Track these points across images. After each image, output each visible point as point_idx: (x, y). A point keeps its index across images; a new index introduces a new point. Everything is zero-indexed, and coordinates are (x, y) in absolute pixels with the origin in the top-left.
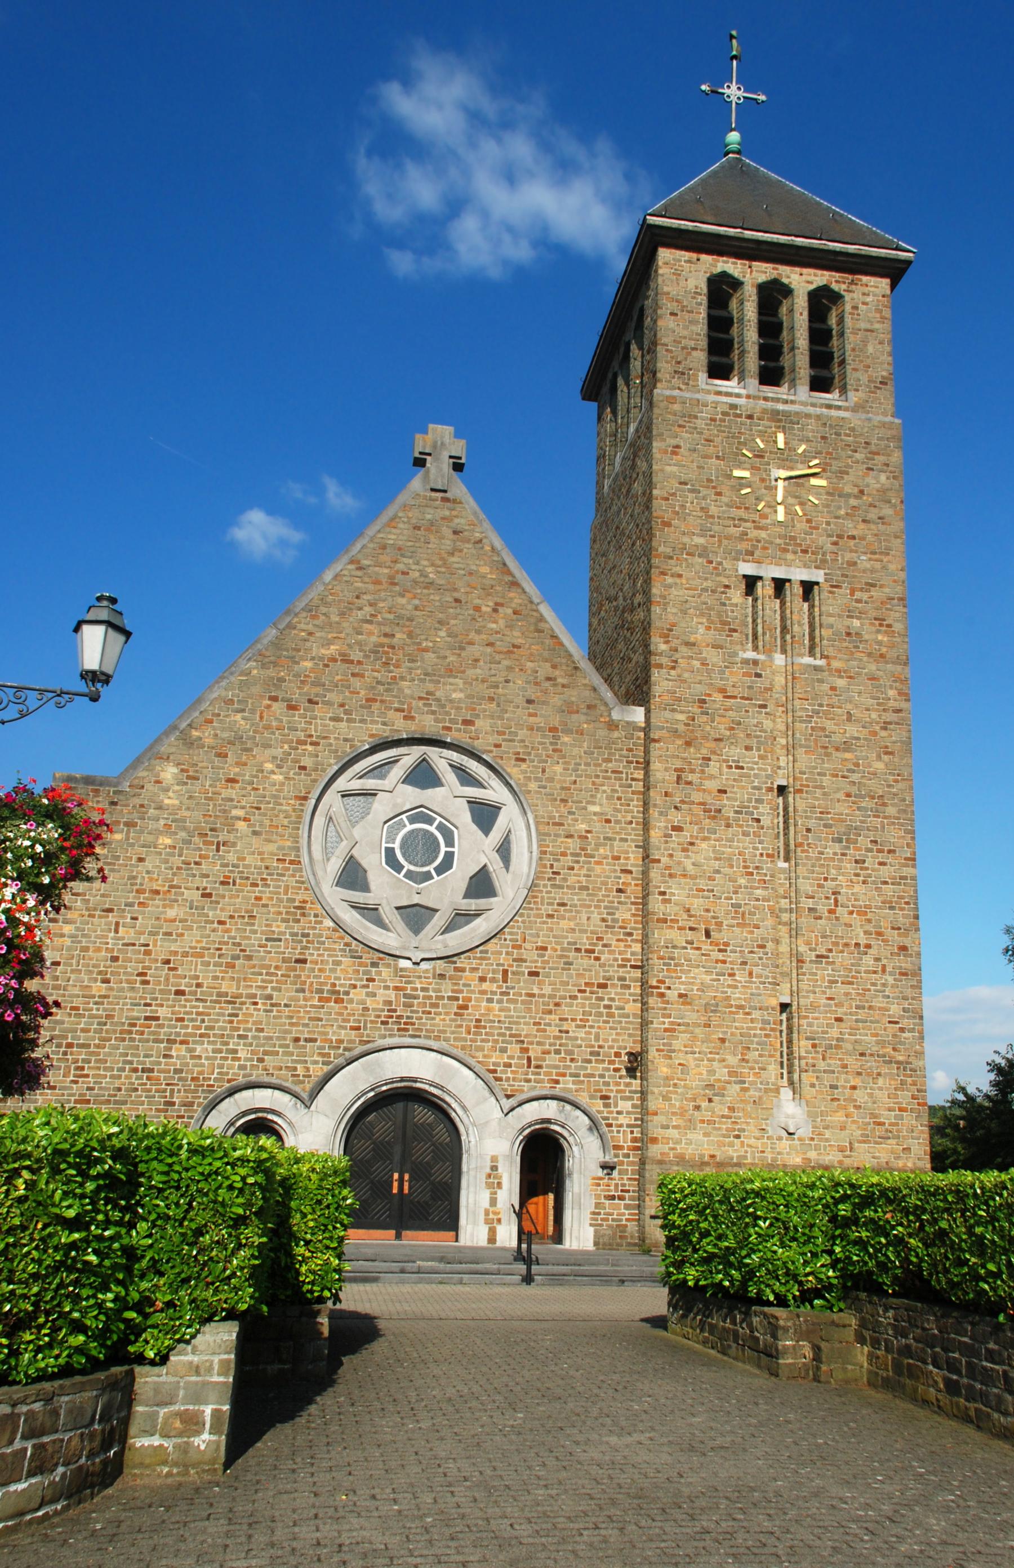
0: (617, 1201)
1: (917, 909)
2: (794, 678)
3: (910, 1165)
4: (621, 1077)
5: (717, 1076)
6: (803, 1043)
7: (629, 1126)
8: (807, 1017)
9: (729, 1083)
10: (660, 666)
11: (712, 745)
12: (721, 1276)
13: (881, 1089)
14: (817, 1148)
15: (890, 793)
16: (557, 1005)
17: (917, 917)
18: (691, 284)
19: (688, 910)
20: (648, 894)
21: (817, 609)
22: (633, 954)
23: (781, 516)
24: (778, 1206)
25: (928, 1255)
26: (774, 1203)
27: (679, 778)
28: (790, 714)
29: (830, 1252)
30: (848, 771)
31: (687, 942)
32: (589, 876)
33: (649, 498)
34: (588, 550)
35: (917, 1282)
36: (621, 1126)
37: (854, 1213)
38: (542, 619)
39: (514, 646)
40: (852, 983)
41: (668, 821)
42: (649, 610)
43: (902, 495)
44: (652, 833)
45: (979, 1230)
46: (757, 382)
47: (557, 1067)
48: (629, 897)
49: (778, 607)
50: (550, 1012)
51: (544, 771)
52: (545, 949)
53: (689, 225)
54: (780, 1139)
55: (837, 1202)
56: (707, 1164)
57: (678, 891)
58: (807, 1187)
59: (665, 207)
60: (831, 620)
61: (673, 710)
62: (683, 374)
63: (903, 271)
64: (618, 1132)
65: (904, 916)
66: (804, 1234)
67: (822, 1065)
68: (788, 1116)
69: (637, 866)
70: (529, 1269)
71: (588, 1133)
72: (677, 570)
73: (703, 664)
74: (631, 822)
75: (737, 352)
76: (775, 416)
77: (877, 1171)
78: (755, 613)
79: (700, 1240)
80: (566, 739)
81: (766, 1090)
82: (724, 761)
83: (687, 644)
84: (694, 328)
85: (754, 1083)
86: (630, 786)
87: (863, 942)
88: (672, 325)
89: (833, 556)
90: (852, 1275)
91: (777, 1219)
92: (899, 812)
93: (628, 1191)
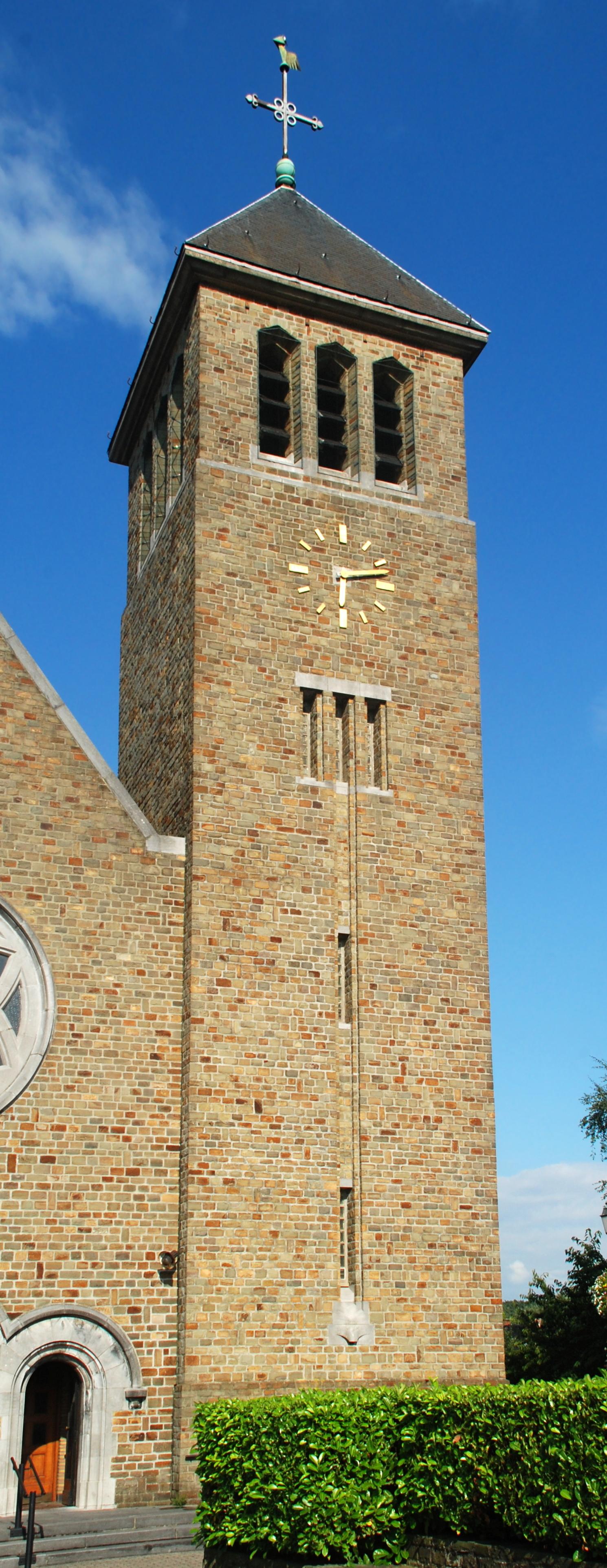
0: (145, 1441)
1: (491, 1077)
2: (357, 811)
3: (483, 1374)
4: (153, 1284)
5: (268, 1278)
6: (366, 1234)
7: (162, 1344)
8: (370, 1204)
9: (282, 1285)
10: (204, 790)
11: (264, 884)
12: (266, 1529)
13: (451, 1285)
14: (381, 1359)
15: (462, 945)
16: (76, 1197)
17: (491, 1086)
18: (240, 336)
19: (236, 1080)
20: (188, 1061)
21: (383, 732)
22: (170, 1132)
23: (343, 621)
24: (334, 1435)
25: (499, 1484)
26: (329, 1431)
27: (226, 922)
28: (353, 852)
29: (392, 1488)
30: (418, 918)
31: (234, 1117)
32: (118, 1039)
33: (192, 589)
34: (119, 646)
35: (488, 1520)
36: (153, 1344)
37: (419, 1439)
38: (60, 726)
39: (26, 757)
40: (420, 1163)
41: (213, 974)
42: (191, 723)
43: (476, 607)
44: (194, 988)
45: (552, 1450)
46: (316, 462)
47: (76, 1275)
48: (166, 1064)
49: (340, 727)
50: (68, 1207)
51: (63, 911)
52: (63, 1128)
53: (237, 265)
54: (339, 1350)
55: (401, 1425)
56: (255, 1386)
57: (224, 1057)
58: (367, 1409)
59: (207, 237)
60: (399, 745)
61: (219, 843)
62: (231, 443)
63: (479, 351)
64: (150, 1352)
65: (478, 1086)
66: (363, 1468)
67: (387, 1260)
68: (348, 1322)
69: (175, 1026)
70: (30, 1546)
71: (112, 1356)
72: (225, 676)
73: (254, 790)
74: (169, 975)
75: (293, 424)
76: (337, 504)
77: (445, 1384)
78: (314, 732)
79: (243, 1484)
80: (91, 873)
81: (325, 1292)
82: (279, 904)
83: (236, 765)
84: (243, 390)
85: (311, 1284)
86: (168, 931)
87: (433, 1115)
88: (217, 383)
89: (402, 672)
90: (416, 1516)
91: (332, 1451)
92: (472, 966)
93: (160, 1427)
